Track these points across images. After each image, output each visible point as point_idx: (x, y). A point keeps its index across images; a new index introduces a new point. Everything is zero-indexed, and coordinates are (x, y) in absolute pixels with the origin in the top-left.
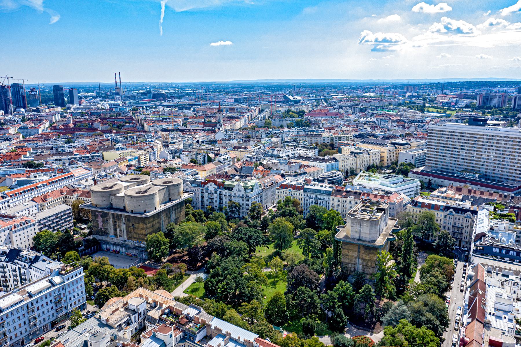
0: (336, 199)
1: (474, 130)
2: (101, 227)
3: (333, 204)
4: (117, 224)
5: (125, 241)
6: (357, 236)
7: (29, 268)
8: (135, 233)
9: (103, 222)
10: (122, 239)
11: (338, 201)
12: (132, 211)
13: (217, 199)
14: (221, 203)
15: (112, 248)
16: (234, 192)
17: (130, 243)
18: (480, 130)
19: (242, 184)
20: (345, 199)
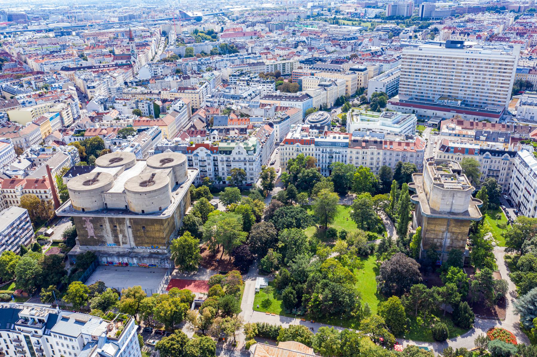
0: (354, 151)
1: (453, 53)
2: (93, 234)
3: (351, 157)
4: (118, 228)
5: (133, 248)
6: (447, 209)
7: (44, 334)
8: (148, 237)
9: (95, 229)
10: (127, 246)
11: (358, 153)
12: (143, 211)
13: (211, 167)
14: (216, 170)
15: (116, 260)
16: (234, 155)
17: (140, 250)
18: (460, 54)
19: (242, 145)
20: (365, 150)
